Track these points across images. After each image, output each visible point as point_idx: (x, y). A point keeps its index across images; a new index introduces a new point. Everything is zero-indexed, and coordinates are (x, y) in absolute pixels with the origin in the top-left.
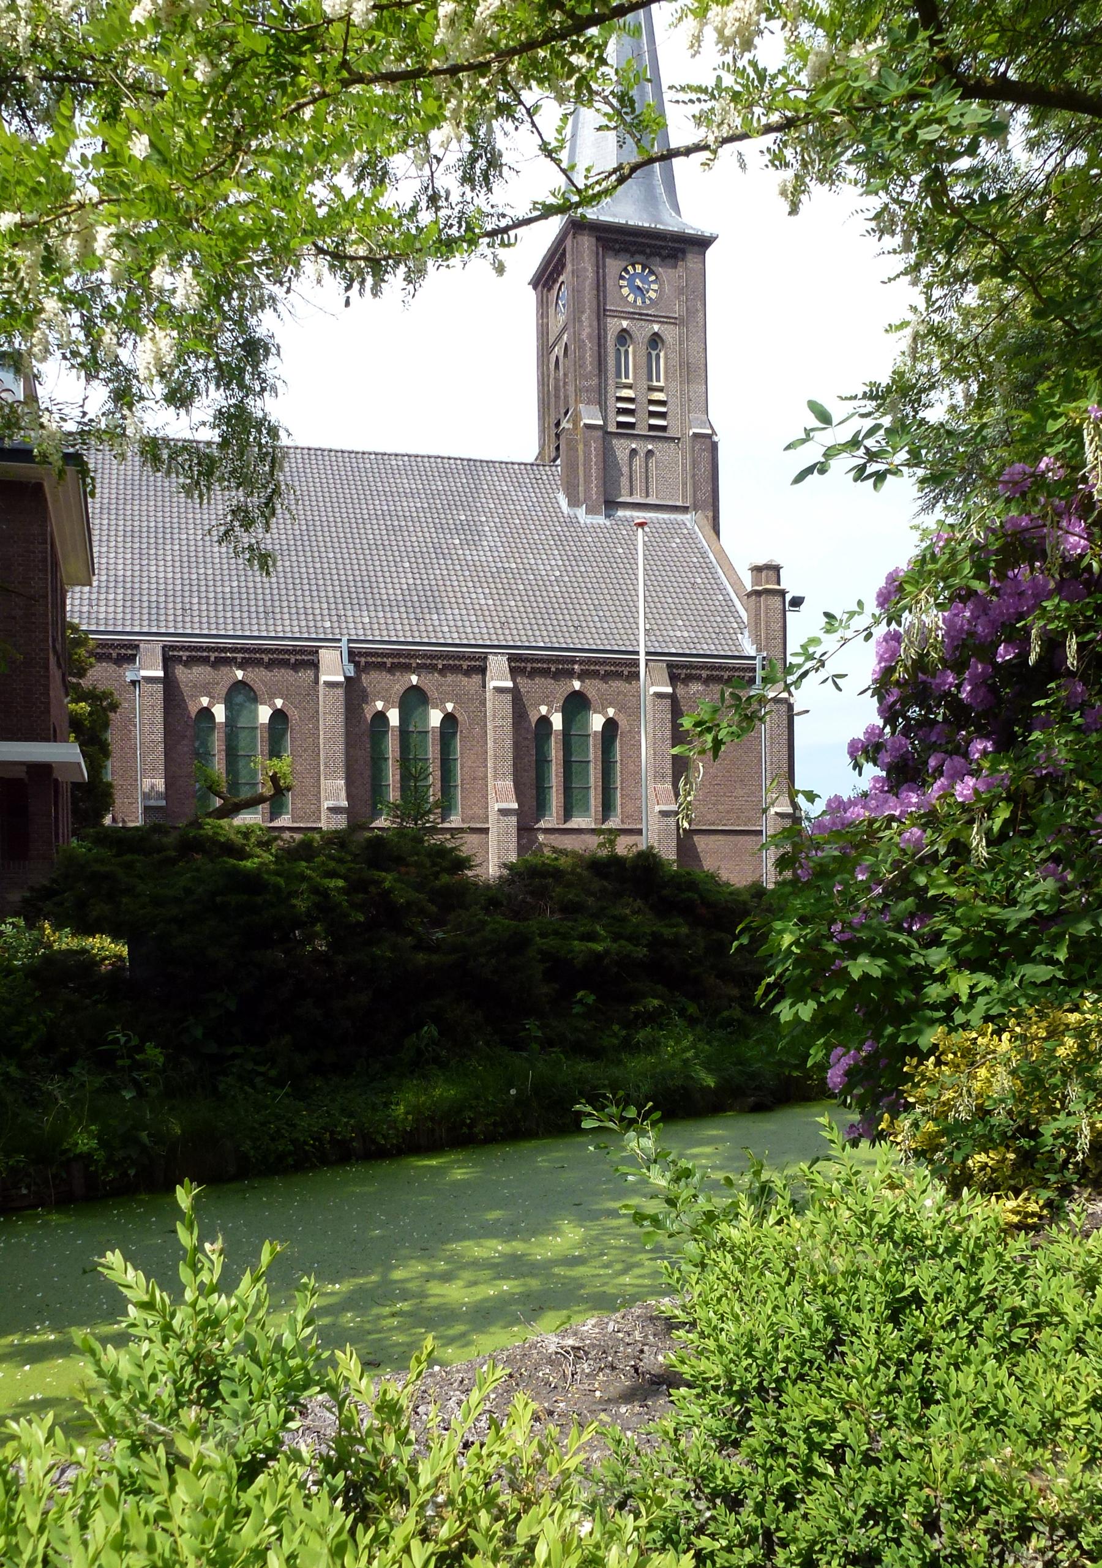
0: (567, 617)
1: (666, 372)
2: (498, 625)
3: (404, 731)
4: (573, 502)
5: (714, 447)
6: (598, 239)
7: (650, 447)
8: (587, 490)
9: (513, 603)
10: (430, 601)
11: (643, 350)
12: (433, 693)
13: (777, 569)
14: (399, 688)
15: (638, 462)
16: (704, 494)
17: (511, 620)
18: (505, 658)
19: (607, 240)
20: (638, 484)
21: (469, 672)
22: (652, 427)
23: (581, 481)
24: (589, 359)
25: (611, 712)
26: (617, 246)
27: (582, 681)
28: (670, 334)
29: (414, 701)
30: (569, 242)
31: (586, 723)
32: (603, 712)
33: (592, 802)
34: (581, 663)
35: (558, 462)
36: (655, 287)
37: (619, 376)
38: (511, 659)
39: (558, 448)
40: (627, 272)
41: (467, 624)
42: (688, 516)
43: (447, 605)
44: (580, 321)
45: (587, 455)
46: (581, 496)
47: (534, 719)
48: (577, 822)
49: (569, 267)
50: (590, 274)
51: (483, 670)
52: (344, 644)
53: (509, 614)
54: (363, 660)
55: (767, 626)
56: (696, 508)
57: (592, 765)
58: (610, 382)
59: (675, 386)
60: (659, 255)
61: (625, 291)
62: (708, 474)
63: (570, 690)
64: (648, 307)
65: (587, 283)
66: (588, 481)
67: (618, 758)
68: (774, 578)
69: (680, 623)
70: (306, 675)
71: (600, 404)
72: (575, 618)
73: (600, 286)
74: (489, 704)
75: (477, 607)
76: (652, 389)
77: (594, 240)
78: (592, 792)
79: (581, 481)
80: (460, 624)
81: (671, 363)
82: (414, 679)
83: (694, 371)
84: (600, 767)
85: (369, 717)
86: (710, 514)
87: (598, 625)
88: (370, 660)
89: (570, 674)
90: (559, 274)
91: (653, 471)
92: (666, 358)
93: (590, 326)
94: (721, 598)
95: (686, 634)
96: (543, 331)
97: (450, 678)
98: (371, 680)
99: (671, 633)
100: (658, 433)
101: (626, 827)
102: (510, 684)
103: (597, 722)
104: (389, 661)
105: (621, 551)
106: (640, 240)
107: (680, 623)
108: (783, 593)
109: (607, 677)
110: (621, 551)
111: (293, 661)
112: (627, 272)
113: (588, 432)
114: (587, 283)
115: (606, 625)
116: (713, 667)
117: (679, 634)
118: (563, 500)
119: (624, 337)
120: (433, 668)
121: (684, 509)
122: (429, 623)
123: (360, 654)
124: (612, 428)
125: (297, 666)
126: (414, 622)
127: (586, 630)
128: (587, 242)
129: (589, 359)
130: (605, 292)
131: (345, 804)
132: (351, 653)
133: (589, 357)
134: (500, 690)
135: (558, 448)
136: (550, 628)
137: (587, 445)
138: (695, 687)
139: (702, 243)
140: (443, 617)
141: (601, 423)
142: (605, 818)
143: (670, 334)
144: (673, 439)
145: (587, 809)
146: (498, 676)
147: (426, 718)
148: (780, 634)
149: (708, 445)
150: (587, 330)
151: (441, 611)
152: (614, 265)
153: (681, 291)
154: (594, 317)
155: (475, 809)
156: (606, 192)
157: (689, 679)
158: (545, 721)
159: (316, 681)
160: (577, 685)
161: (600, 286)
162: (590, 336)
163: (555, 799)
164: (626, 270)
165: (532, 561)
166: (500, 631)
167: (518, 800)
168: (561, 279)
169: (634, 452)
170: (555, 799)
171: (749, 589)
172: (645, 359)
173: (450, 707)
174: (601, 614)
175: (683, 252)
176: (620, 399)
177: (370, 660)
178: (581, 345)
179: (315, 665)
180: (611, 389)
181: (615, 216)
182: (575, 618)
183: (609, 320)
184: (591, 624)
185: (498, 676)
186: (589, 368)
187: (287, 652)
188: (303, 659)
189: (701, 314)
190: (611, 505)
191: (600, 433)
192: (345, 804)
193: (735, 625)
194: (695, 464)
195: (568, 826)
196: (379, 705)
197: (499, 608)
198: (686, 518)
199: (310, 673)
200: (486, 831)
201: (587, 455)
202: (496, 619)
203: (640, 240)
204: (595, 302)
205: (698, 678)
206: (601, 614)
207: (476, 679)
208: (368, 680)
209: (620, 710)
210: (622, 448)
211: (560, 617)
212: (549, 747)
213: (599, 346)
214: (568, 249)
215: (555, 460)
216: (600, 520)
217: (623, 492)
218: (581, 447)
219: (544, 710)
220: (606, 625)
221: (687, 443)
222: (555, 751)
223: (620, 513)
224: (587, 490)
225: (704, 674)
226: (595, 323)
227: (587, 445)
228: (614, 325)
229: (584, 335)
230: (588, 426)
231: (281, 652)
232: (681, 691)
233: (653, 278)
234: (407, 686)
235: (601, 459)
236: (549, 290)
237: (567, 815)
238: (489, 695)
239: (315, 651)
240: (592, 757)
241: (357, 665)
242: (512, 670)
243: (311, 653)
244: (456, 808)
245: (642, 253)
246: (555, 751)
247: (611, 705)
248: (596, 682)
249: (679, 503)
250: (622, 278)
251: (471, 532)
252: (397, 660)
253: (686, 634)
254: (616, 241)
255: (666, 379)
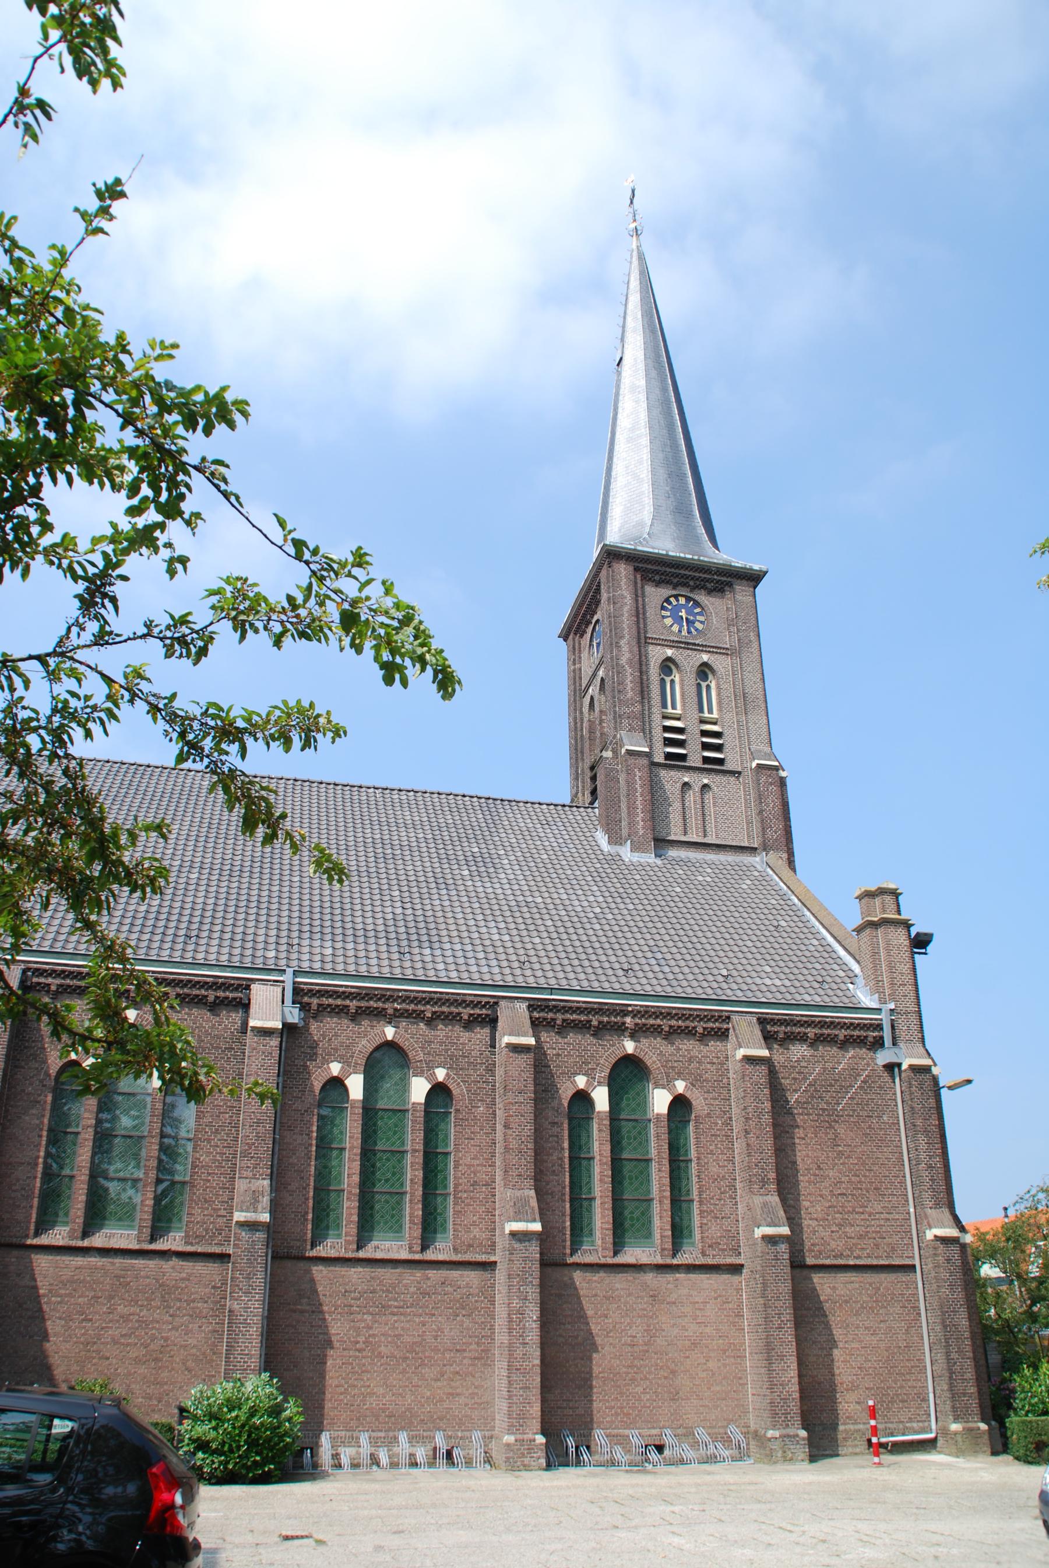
0: (613, 959)
1: (720, 703)
2: (516, 965)
3: (369, 1110)
4: (615, 839)
5: (782, 782)
6: (636, 569)
7: (706, 781)
8: (632, 824)
9: (537, 940)
10: (425, 934)
11: (691, 679)
12: (416, 1054)
13: (895, 894)
14: (366, 1045)
15: (692, 797)
16: (775, 833)
17: (534, 959)
18: (524, 1005)
19: (646, 570)
20: (693, 822)
21: (469, 1024)
22: (706, 760)
23: (624, 814)
24: (630, 686)
25: (680, 1086)
26: (657, 578)
27: (637, 1041)
28: (720, 663)
29: (386, 1062)
30: (603, 574)
31: (643, 1103)
32: (668, 1085)
33: (656, 1222)
34: (635, 1014)
35: (596, 805)
36: (702, 618)
37: (664, 706)
38: (534, 1006)
39: (594, 792)
40: (670, 603)
41: (472, 961)
42: (758, 859)
43: (446, 939)
44: (618, 647)
45: (630, 784)
46: (625, 832)
47: (566, 1093)
48: (631, 1255)
49: (604, 596)
50: (629, 599)
51: (492, 1022)
52: (288, 978)
53: (532, 952)
54: (315, 1001)
55: (891, 968)
56: (765, 848)
57: (654, 1166)
58: (654, 710)
59: (730, 717)
60: (704, 588)
61: (668, 621)
62: (778, 809)
63: (620, 1054)
64: (695, 637)
65: (626, 609)
66: (632, 814)
67: (693, 1154)
68: (894, 907)
69: (768, 969)
70: (231, 1019)
71: (643, 731)
72: (623, 959)
73: (639, 614)
74: (499, 1072)
75: (487, 943)
76: (703, 721)
77: (631, 568)
78: (656, 1207)
79: (624, 814)
80: (461, 961)
81: (724, 694)
82: (390, 1032)
83: (751, 701)
84: (666, 1167)
85: (317, 1086)
86: (785, 856)
87: (657, 968)
88: (325, 1001)
89: (620, 1029)
90: (594, 613)
91: (711, 810)
92: (718, 688)
93: (631, 651)
94: (815, 942)
95: (778, 982)
96: (575, 677)
97: (442, 1031)
98: (327, 1030)
99: (758, 981)
100: (714, 765)
101: (710, 1261)
102: (532, 1041)
103: (660, 1101)
104: (353, 1004)
105: (678, 889)
106: (682, 572)
107: (768, 969)
108: (907, 925)
109: (671, 1034)
110: (678, 889)
111: (211, 998)
112: (670, 603)
113: (631, 761)
114: (626, 609)
115: (666, 969)
116: (822, 1024)
117: (768, 982)
118: (602, 839)
119: (668, 666)
120: (419, 1016)
121: (753, 850)
122: (417, 958)
123: (312, 993)
124: (659, 758)
125: (215, 1006)
126: (396, 956)
127: (640, 974)
128: (623, 570)
129: (630, 686)
130: (645, 619)
131: (265, 1217)
132: (297, 991)
133: (630, 690)
134: (516, 1049)
135: (594, 792)
136: (589, 970)
137: (629, 772)
138: (799, 1051)
139: (754, 578)
140: (438, 952)
141: (647, 750)
142: (675, 1251)
143: (720, 663)
144: (732, 773)
145: (649, 1235)
146: (515, 1031)
147: (404, 1088)
148: (908, 978)
149: (773, 780)
150: (630, 678)
151: (436, 945)
152: (655, 594)
153: (730, 623)
154: (634, 643)
155: (476, 1232)
156: (638, 622)
157: (790, 1038)
158: (582, 1098)
159: (245, 1023)
160: (630, 1046)
161: (639, 614)
162: (630, 662)
163: (601, 1218)
164: (667, 600)
165: (565, 896)
166: (518, 972)
167: (542, 1220)
168: (595, 618)
169: (686, 785)
170: (601, 1218)
171: (858, 921)
172: (694, 689)
173: (441, 1074)
174: (659, 956)
175: (730, 585)
176: (666, 729)
177: (325, 1001)
178: (619, 670)
179: (245, 1006)
180: (657, 717)
181: (653, 548)
182: (623, 959)
183: (651, 648)
184: (647, 968)
185: (515, 1031)
186: (630, 694)
187: (204, 985)
188: (232, 997)
189: (755, 645)
190: (661, 843)
191: (645, 761)
192: (265, 1217)
193: (841, 974)
194: (760, 798)
195: (620, 1259)
196: (335, 1068)
197: (519, 945)
198: (756, 860)
199: (236, 1017)
200: (489, 1266)
201: (630, 784)
202: (513, 958)
203: (682, 572)
204: (635, 627)
205: (803, 1038)
206: (659, 956)
207: (482, 1033)
208: (323, 1029)
209: (695, 1081)
210: (671, 780)
211: (603, 958)
212: (589, 1136)
213: (641, 672)
214: (603, 580)
215: (592, 803)
216: (650, 858)
217: (673, 830)
218: (622, 777)
219: (581, 1081)
220: (666, 969)
221: (748, 778)
222: (599, 1145)
223: (673, 853)
224: (632, 824)
225: (811, 1032)
226: (636, 649)
227: (629, 772)
228: (656, 654)
229: (623, 660)
230: (630, 753)
231: (195, 985)
232: (779, 1057)
233: (698, 610)
234: (379, 1041)
235: (647, 788)
236: (582, 636)
237: (618, 1247)
238: (501, 1056)
239: (245, 986)
240: (653, 1153)
241: (304, 1008)
242: (535, 1024)
243: (237, 988)
244: (445, 1230)
245: (685, 585)
246: (599, 1145)
247: (680, 1075)
248: (658, 1041)
249: (746, 844)
250: (663, 608)
251: (484, 865)
252: (367, 1005)
253: (778, 982)
254: (657, 572)
255: (720, 710)
